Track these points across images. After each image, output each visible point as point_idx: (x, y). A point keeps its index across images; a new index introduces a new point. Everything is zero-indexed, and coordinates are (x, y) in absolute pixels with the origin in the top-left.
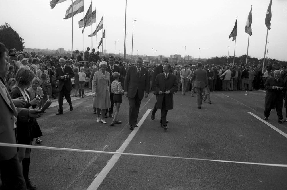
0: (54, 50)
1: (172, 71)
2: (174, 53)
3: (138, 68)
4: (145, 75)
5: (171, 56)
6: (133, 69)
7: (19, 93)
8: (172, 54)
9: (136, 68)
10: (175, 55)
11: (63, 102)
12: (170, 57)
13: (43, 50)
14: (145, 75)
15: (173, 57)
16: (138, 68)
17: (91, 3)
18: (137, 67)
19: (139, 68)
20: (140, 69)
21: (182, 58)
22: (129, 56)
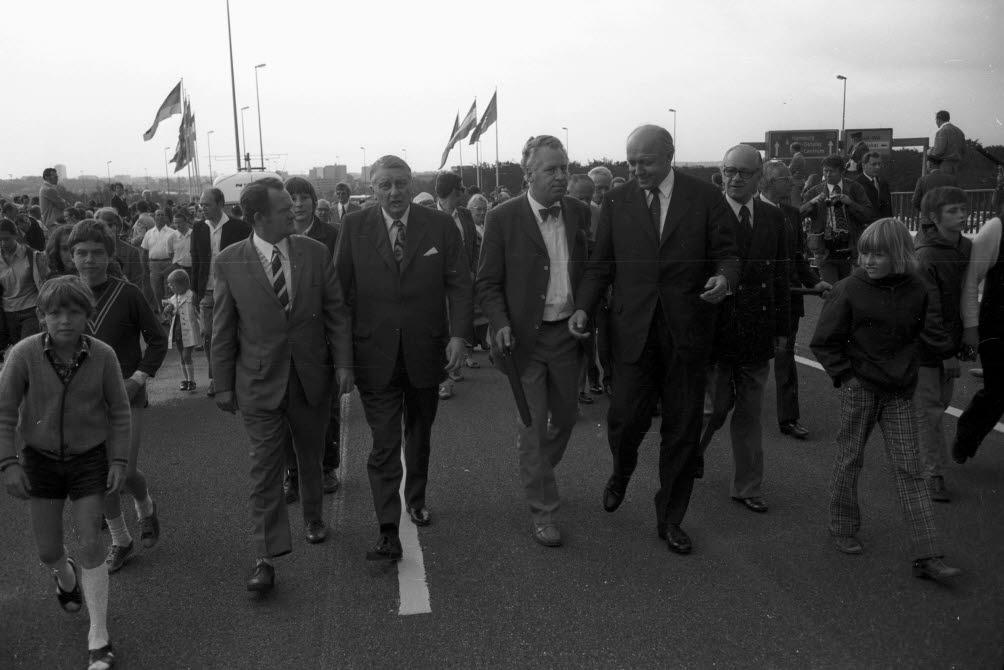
0: (128, 176)
1: (944, 240)
2: (330, 161)
3: (390, 221)
4: (433, 251)
5: (314, 171)
6: (365, 222)
7: (80, 293)
8: (318, 165)
9: (384, 220)
10: (327, 169)
11: (994, 424)
12: (359, 171)
13: (136, 179)
14: (433, 251)
15: (321, 175)
16: (390, 221)
17: (492, 96)
18: (388, 212)
19: (397, 216)
20: (404, 220)
21: (350, 177)
22: (157, 181)
